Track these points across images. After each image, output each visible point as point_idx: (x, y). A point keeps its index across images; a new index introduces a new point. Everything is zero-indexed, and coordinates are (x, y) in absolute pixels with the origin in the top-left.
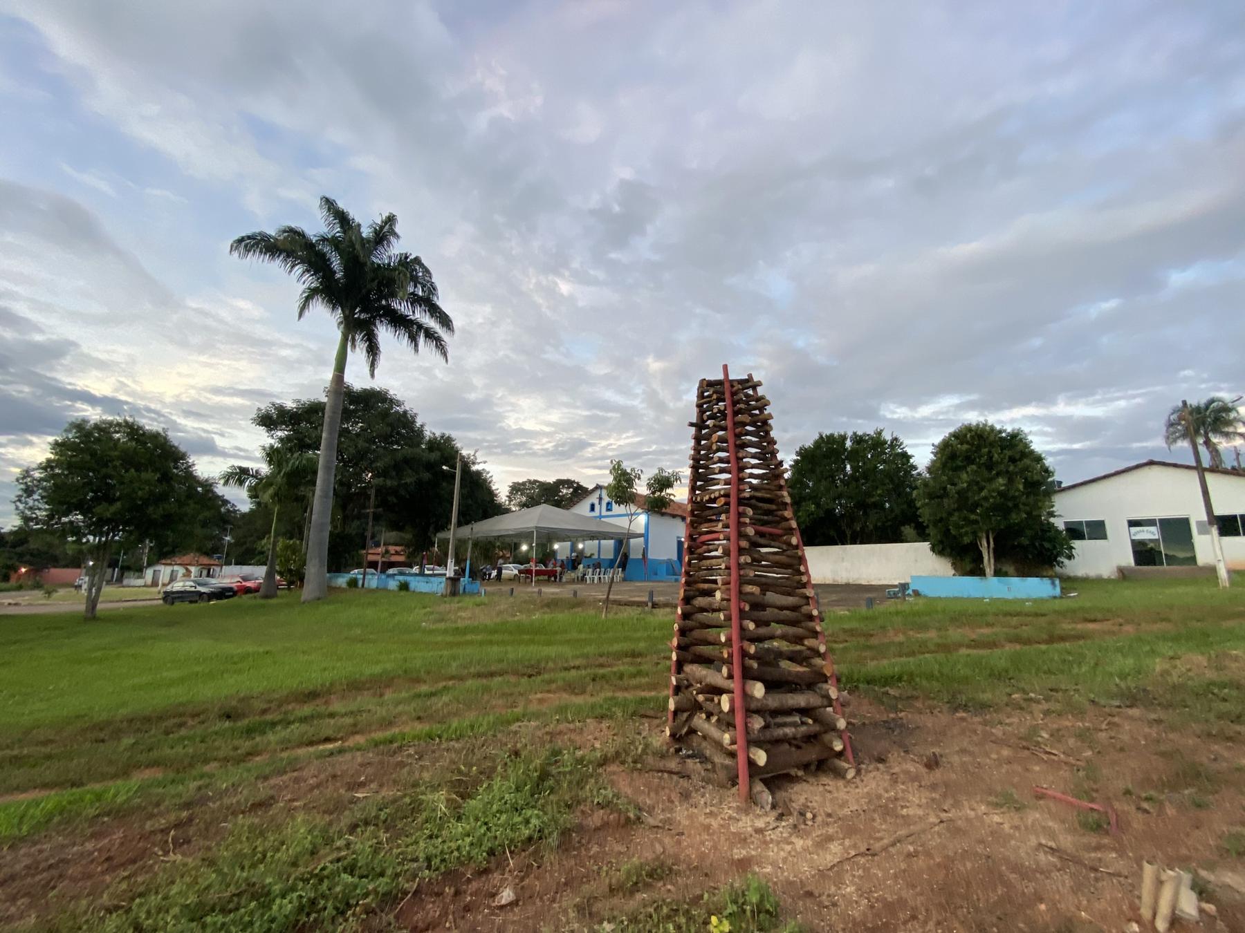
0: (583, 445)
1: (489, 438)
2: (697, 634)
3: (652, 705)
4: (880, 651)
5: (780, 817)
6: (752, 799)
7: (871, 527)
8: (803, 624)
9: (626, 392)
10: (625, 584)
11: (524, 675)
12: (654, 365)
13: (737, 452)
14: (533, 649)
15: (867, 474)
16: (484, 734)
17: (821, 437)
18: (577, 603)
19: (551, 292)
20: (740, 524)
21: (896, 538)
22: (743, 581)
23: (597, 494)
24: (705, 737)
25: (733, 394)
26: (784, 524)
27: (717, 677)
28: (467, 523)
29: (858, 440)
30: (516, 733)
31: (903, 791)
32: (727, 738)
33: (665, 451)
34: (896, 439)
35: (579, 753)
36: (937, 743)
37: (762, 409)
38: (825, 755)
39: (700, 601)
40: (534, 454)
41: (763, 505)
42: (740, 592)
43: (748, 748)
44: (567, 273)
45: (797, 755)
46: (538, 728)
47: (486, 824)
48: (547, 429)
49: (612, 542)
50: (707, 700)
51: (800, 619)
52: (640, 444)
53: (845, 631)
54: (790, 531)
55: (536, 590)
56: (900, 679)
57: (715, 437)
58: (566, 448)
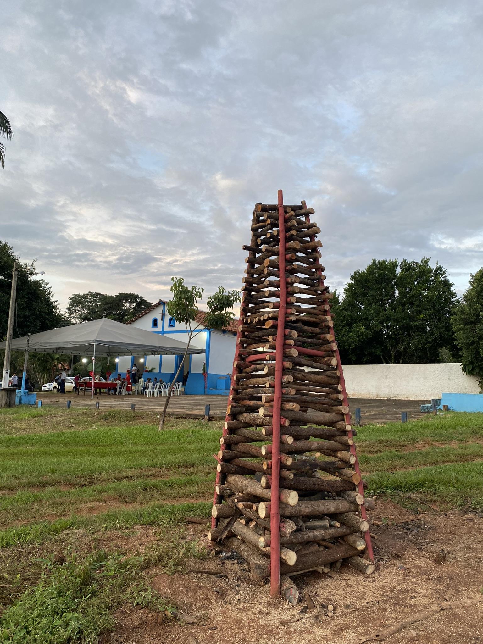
0: (147, 259)
1: (49, 248)
2: (241, 447)
3: (198, 512)
4: (409, 461)
5: (304, 610)
6: (281, 595)
7: (413, 348)
8: (338, 438)
9: (193, 207)
10: (186, 397)
11: (75, 485)
12: (223, 183)
13: (286, 278)
14: (87, 460)
15: (411, 300)
16: (32, 542)
17: (374, 263)
18: (135, 416)
19: (119, 98)
20: (285, 346)
21: (434, 358)
22: (285, 399)
23: (160, 310)
24: (243, 541)
25: (286, 221)
26: (326, 347)
27: (256, 487)
28: (24, 334)
29: (407, 267)
30: (64, 540)
31: (413, 583)
32: (262, 541)
33: (222, 270)
34: (440, 268)
35: (123, 558)
36: (446, 541)
37: (312, 236)
38: (350, 553)
39: (246, 417)
40: (97, 266)
41: (307, 331)
42: (282, 409)
43: (281, 549)
44: (135, 80)
45: (324, 555)
46: (85, 535)
47: (26, 628)
48: (110, 241)
49: (174, 357)
50: (246, 507)
51: (335, 434)
52: (206, 261)
53: (381, 442)
54: (331, 353)
55: (94, 402)
56: (422, 485)
57: (267, 262)
58: (130, 262)
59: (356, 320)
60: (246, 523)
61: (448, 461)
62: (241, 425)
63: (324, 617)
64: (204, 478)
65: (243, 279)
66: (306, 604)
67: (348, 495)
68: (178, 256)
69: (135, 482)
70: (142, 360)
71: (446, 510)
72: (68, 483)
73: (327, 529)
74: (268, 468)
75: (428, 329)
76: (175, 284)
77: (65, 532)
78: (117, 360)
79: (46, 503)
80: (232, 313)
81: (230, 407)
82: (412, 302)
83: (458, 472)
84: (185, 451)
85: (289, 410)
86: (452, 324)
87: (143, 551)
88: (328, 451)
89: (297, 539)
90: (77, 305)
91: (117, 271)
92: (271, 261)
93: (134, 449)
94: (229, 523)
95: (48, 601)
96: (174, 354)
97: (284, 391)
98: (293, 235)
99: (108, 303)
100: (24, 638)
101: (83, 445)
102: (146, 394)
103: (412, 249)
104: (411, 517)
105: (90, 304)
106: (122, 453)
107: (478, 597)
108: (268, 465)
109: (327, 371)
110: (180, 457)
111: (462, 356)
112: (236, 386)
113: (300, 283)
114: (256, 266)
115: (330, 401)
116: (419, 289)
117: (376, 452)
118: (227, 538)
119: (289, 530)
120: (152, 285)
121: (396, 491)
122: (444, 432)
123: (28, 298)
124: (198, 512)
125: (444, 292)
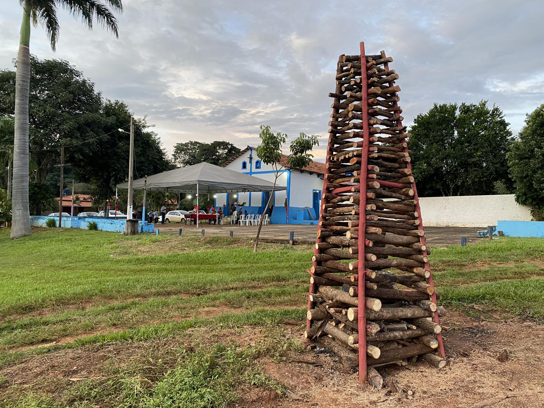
0: (234, 112)
1: (155, 105)
2: (330, 264)
3: (294, 316)
4: (470, 277)
5: (389, 393)
6: (368, 381)
8: (414, 257)
10: (271, 226)
11: (193, 294)
12: (297, 42)
15: (469, 139)
16: (165, 336)
18: (233, 241)
20: (369, 179)
22: (369, 224)
24: (334, 339)
25: (368, 69)
29: (466, 110)
30: (190, 336)
31: (481, 376)
34: (497, 109)
35: (238, 350)
37: (391, 82)
38: (425, 351)
39: (334, 239)
40: (194, 120)
42: (366, 233)
43: (367, 346)
45: (403, 352)
46: (206, 332)
48: (204, 98)
50: (336, 312)
51: (412, 253)
52: (283, 111)
53: (444, 262)
56: (484, 298)
57: (351, 106)
59: (419, 158)
60: (336, 325)
61: (506, 278)
62: (330, 246)
63: (405, 400)
64: (295, 290)
65: (329, 123)
66: (389, 389)
67: (423, 304)
68: (260, 108)
69: (240, 292)
70: (235, 196)
71: (505, 318)
72: (187, 292)
73: (405, 330)
74: (355, 280)
75: (484, 164)
76: (263, 131)
77: (190, 329)
78: (215, 196)
79: (172, 308)
80: (311, 155)
81: (320, 231)
82: (470, 140)
83: (516, 287)
84: (277, 268)
85: (372, 233)
86: (507, 160)
87: (254, 345)
88: (405, 268)
89: (380, 337)
90: (181, 152)
91: (211, 123)
92: (355, 106)
93: (235, 266)
94: (322, 324)
95: (186, 380)
96: (261, 191)
97: (368, 217)
98: (374, 81)
99: (205, 150)
100: (171, 406)
101: (195, 264)
102: (240, 224)
103: (468, 94)
104: (475, 324)
105: (190, 151)
106: (227, 270)
107: (539, 389)
108: (355, 278)
109: (404, 200)
110: (274, 273)
111: (516, 188)
112: (324, 214)
113: (381, 124)
114: (340, 111)
115: (408, 225)
116: (477, 129)
117: (440, 270)
118: (321, 336)
119: (374, 331)
120: (240, 134)
121: (460, 302)
122: (501, 254)
123: (142, 147)
124: (294, 316)
125: (501, 131)
